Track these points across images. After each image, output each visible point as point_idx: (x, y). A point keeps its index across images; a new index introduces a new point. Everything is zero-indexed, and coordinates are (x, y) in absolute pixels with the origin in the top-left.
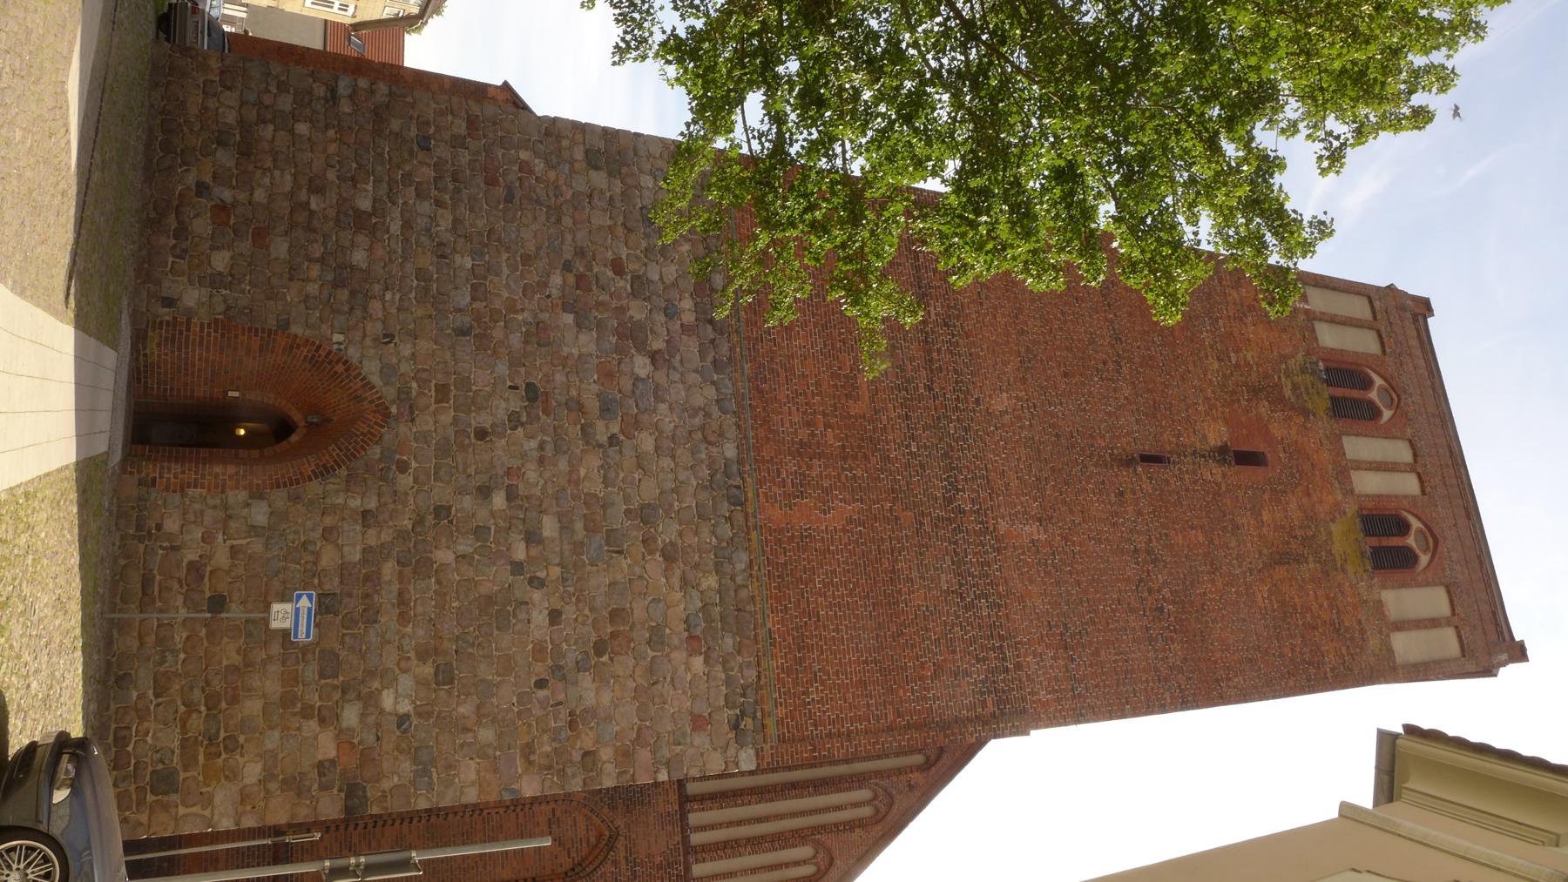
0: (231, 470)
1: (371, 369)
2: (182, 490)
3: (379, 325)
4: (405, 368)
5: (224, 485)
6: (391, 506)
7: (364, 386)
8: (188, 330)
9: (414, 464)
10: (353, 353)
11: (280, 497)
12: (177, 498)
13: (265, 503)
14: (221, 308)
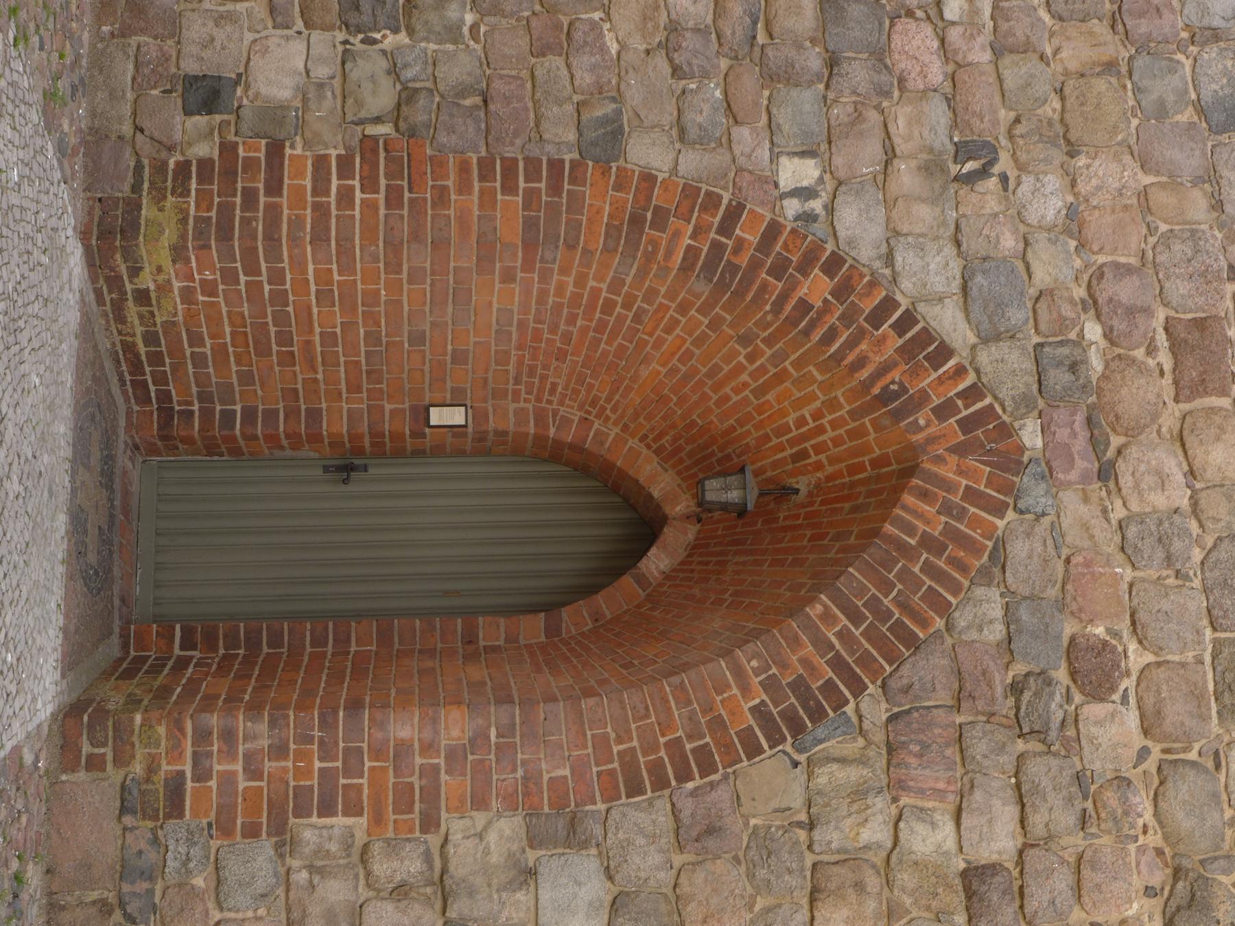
0: (455, 726)
1: (927, 277)
2: (279, 827)
3: (938, 113)
4: (1053, 266)
5: (431, 795)
6: (1075, 842)
7: (908, 352)
8: (274, 187)
9: (1137, 658)
10: (858, 228)
11: (641, 828)
12: (257, 861)
13: (587, 864)
14: (382, 98)
